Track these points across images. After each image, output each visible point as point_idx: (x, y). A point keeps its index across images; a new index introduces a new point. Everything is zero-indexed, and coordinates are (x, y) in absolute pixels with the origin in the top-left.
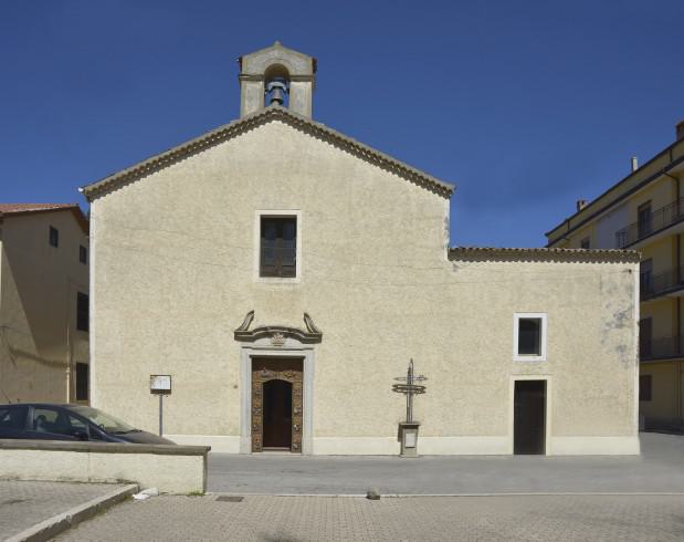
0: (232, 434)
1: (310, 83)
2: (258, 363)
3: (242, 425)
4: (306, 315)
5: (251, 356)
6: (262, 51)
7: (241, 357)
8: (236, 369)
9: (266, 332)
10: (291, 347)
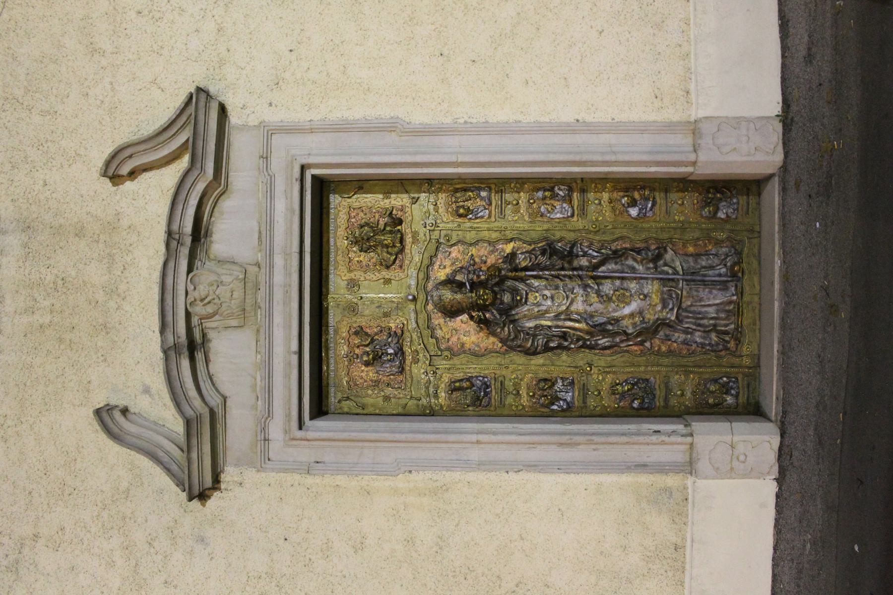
3: (643, 467)
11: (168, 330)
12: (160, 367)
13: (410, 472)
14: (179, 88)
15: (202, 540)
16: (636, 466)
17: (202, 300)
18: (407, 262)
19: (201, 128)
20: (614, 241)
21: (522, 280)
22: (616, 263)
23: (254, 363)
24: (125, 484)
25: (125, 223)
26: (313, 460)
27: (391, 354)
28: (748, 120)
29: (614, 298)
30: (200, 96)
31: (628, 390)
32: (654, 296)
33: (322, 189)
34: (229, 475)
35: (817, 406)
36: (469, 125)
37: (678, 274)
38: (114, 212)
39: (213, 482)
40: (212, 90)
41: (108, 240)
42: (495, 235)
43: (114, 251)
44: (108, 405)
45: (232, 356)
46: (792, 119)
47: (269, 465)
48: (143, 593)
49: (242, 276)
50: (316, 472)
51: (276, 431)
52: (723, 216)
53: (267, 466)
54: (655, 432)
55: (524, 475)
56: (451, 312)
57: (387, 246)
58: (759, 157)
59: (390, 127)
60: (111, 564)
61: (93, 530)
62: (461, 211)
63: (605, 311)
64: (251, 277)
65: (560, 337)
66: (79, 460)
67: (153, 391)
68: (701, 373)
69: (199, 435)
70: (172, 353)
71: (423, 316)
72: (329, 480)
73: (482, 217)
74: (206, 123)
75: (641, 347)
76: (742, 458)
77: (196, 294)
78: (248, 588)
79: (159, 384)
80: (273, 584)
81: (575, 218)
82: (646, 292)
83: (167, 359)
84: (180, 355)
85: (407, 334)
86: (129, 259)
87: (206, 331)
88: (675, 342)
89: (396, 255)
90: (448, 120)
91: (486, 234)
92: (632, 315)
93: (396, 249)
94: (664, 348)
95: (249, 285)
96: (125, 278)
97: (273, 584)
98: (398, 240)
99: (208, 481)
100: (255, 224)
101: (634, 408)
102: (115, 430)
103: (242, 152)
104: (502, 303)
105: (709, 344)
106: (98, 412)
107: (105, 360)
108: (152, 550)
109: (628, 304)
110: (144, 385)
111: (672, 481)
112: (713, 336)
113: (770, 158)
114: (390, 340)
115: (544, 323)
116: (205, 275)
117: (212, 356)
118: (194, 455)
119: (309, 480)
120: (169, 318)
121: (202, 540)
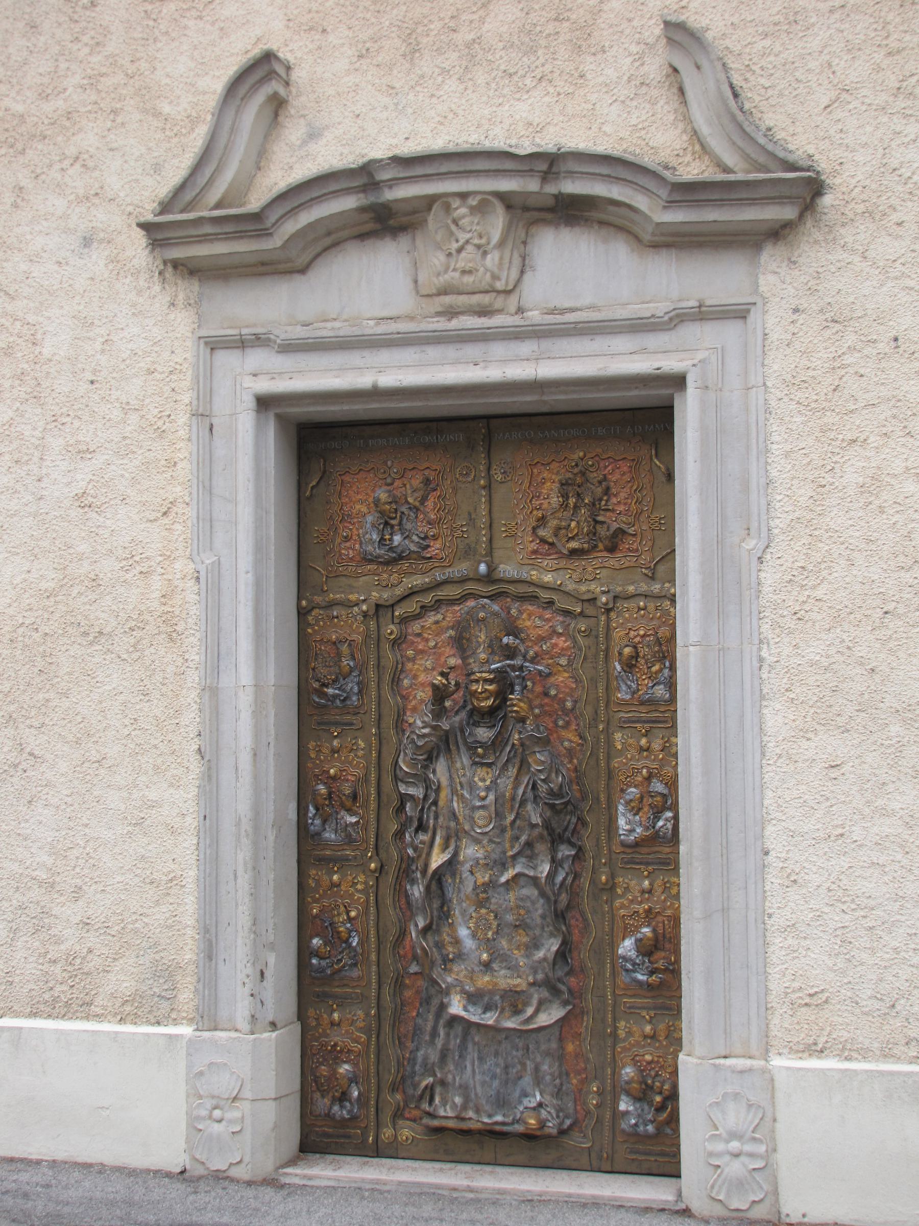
0: (132, 1009)
1: (623, 1097)
2: (322, 444)
3: (210, 951)
4: (679, 34)
5: (264, 403)
6: (467, 1168)
7: (204, 417)
8: (248, 976)
9: (380, 207)
10: (580, 314)
15: (87, 242)
16: (210, 941)
22: (543, 917)
24: (167, 109)
25: (589, 64)
26: (215, 421)
27: (391, 540)
29: (483, 911)
30: (808, 190)
31: (339, 933)
32: (487, 978)
34: (185, 289)
41: (561, 40)
44: (288, 68)
47: (204, 350)
48: (3, 151)
50: (194, 429)
52: (622, 1107)
53: (202, 346)
54: (262, 973)
55: (196, 767)
60: (44, 96)
61: (95, 59)
63: (462, 895)
65: (420, 820)
66: (201, 24)
67: (312, 147)
68: (368, 1056)
69: (239, 236)
75: (410, 956)
76: (217, 1113)
78: (18, 324)
80: (26, 366)
82: (495, 966)
84: (364, 191)
88: (418, 1014)
92: (457, 942)
95: (486, 299)
97: (26, 366)
98: (574, 545)
100: (586, 301)
102: (243, 90)
105: (414, 1072)
106: (268, 57)
107: (361, 57)
108: (67, 163)
109: (474, 936)
111: (186, 996)
114: (415, 538)
119: (182, 419)
120: (419, 171)
121: (87, 242)
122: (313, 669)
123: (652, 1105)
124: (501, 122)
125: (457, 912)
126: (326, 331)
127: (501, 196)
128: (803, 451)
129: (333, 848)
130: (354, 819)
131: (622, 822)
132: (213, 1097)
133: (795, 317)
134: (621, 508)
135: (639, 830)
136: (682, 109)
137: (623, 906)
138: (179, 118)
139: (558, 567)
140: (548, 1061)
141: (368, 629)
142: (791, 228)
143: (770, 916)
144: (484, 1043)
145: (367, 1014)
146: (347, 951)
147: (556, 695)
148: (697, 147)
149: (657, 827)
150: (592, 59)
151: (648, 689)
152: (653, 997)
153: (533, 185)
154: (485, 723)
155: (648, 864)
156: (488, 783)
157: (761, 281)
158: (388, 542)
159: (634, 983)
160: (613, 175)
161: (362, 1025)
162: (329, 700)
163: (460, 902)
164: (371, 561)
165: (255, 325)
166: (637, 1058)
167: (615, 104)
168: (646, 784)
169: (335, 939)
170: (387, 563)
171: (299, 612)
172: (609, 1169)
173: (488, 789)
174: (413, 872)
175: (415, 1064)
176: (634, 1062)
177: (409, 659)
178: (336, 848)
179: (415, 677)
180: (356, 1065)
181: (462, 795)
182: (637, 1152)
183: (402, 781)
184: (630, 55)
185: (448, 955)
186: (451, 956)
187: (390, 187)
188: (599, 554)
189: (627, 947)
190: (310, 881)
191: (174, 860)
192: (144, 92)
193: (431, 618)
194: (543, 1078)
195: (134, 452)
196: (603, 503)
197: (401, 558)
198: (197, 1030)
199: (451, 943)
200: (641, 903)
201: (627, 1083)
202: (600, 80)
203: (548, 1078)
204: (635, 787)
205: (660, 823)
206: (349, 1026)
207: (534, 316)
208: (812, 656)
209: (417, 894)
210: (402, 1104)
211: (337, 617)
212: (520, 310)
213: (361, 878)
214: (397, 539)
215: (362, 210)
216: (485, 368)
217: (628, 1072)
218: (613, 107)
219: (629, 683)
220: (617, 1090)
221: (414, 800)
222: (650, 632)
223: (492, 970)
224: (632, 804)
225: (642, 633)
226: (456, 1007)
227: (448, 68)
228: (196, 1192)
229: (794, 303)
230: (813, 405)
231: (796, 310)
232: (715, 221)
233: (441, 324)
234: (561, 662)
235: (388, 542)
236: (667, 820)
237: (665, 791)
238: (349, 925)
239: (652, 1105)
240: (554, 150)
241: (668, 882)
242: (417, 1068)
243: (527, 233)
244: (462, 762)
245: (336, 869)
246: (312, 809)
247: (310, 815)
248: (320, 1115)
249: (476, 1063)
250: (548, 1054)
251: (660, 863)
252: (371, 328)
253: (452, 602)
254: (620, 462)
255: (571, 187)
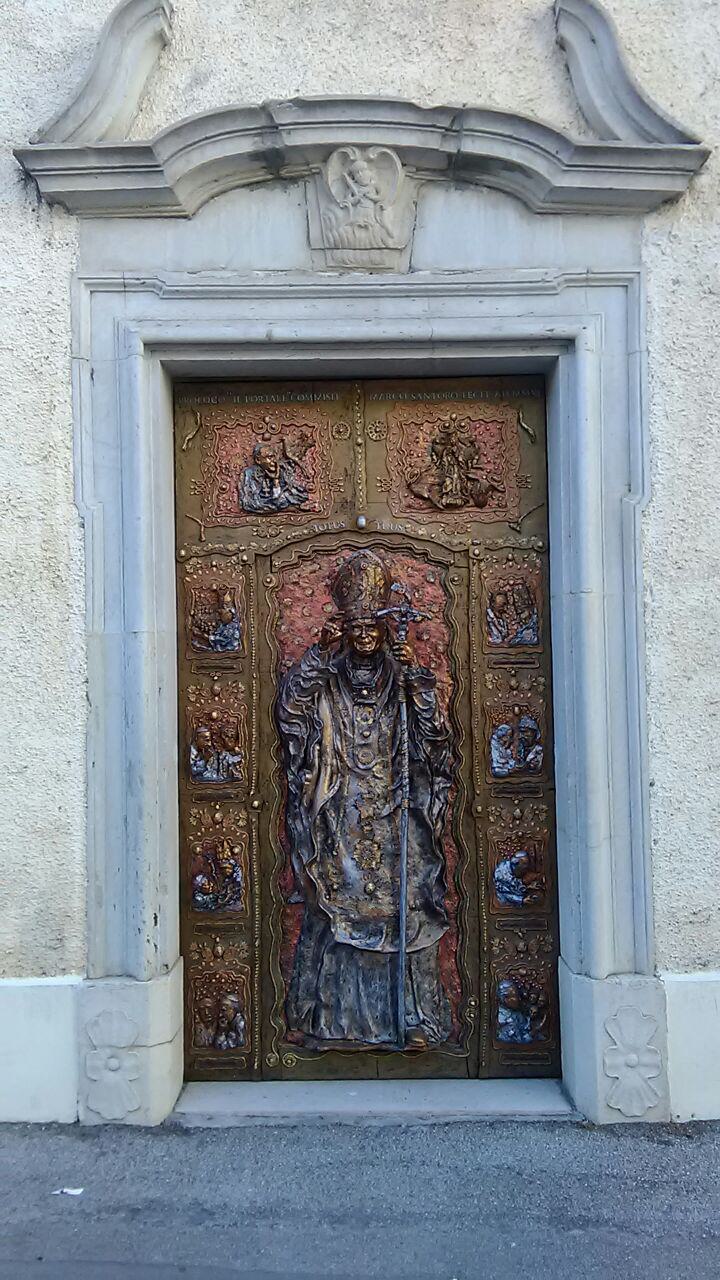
2: (206, 389)
10: (468, 272)
11: (300, 112)
12: (234, 101)
13: (83, 526)
14: (705, 123)
17: (352, 175)
18: (418, 517)
19: (634, 166)
20: (457, 841)
21: (392, 699)
23: (256, 272)
24: (39, 42)
25: (478, 36)
28: (661, 1068)
29: (368, 842)
32: (371, 906)
33: (525, 383)
34: (67, 229)
35: (196, 1203)
36: (640, 610)
37: (409, 945)
38: (496, 16)
39: (49, 194)
40: (703, 180)
42: (461, 655)
43: (430, 18)
45: (263, 231)
46: (668, 1143)
49: (391, 243)
51: (140, 305)
52: (501, 1019)
56: (340, 588)
57: (441, 484)
58: (602, 1084)
59: (631, 480)
62: (499, 599)
64: (390, 259)
67: (197, 93)
69: (126, 171)
70: (262, 122)
71: (332, 543)
72: (64, 393)
73: (490, 634)
74: (646, 171)
75: (291, 887)
76: (114, 1063)
77: (361, 164)
79: (211, 99)
81: (490, 780)
83: (250, 112)
85: (304, 518)
86: (418, 44)
87: (301, 183)
88: (300, 942)
89: (428, 499)
90: (646, 576)
91: (460, 640)
92: (341, 872)
93: (436, 498)
94: (289, 923)
95: (375, 255)
96: (385, 40)
98: (450, 500)
99: (49, 187)
100: (478, 264)
101: (194, 877)
102: (129, 22)
103: (597, 243)
104: (356, 667)
109: (358, 865)
110: (206, 78)
112: (308, 1005)
113: (601, 1104)
114: (294, 491)
115: (329, 732)
116: (397, 183)
117: (259, 193)
118: (93, 162)
122: (193, 616)
123: (528, 1015)
124: (392, 82)
125: (341, 845)
126: (220, 279)
127: (400, 150)
128: (684, 413)
129: (214, 787)
130: (236, 759)
131: (495, 755)
132: (110, 1046)
133: (675, 288)
134: (490, 467)
135: (512, 762)
136: (568, 85)
137: (496, 833)
138: (53, 52)
139: (431, 520)
140: (428, 978)
141: (248, 578)
142: (672, 203)
143: (655, 842)
144: (368, 967)
145: (251, 945)
146: (231, 885)
147: (428, 639)
148: (583, 123)
149: (528, 760)
150: (481, 29)
151: (517, 633)
152: (525, 915)
153: (433, 142)
154: (366, 666)
155: (519, 793)
156: (370, 722)
157: (644, 252)
158: (267, 495)
159: (508, 904)
160: (515, 136)
161: (246, 955)
162: (211, 646)
163: (344, 834)
164: (249, 513)
165: (138, 270)
166: (512, 972)
167: (505, 74)
168: (516, 720)
169: (226, 879)
170: (265, 515)
171: (176, 561)
172: (487, 1076)
173: (370, 728)
174: (296, 807)
175: (298, 990)
176: (510, 978)
177: (286, 606)
178: (218, 787)
179: (292, 623)
180: (240, 994)
181: (346, 735)
182: (513, 1058)
183: (284, 722)
184: (518, 29)
185: (332, 886)
186: (335, 887)
187: (289, 132)
188: (470, 509)
189: (503, 871)
190: (191, 819)
191: (60, 808)
192: (13, 23)
193: (307, 568)
194: (424, 994)
195: (9, 394)
196: (475, 461)
197: (280, 510)
198: (88, 978)
199: (335, 874)
200: (512, 829)
201: (506, 996)
202: (491, 50)
203: (428, 995)
204: (506, 724)
205: (531, 756)
206: (231, 956)
207: (424, 275)
208: (692, 602)
209: (300, 828)
210: (285, 1028)
211: (216, 566)
212: (412, 270)
213: (243, 815)
214: (277, 491)
215: (255, 156)
216: (378, 324)
217: (505, 986)
218: (501, 78)
219: (500, 628)
220: (496, 1001)
221: (298, 739)
222: (519, 581)
223: (377, 898)
224: (505, 739)
225: (512, 582)
226: (342, 933)
227: (338, 25)
228: (103, 1154)
229: (674, 274)
230: (692, 370)
231: (676, 282)
232: (611, 189)
233: (329, 278)
234: (433, 609)
235: (267, 495)
236: (537, 753)
237: (535, 727)
238: (232, 861)
239: (528, 1015)
240: (460, 106)
241: (536, 809)
242: (300, 993)
243: (418, 194)
244: (344, 703)
245: (218, 807)
246: (194, 752)
247: (193, 757)
248: (204, 1046)
249: (361, 986)
250: (428, 973)
251: (530, 792)
252: (260, 279)
253: (329, 553)
254: (490, 424)
255: (473, 147)
